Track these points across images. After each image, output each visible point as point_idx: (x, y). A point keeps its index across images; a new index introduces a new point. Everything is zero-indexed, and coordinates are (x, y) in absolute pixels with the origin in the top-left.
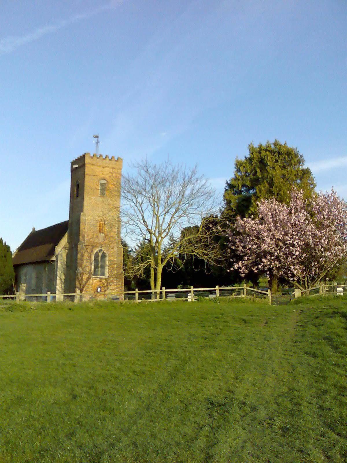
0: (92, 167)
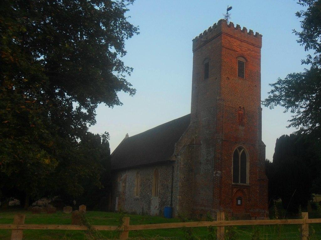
0: (229, 38)
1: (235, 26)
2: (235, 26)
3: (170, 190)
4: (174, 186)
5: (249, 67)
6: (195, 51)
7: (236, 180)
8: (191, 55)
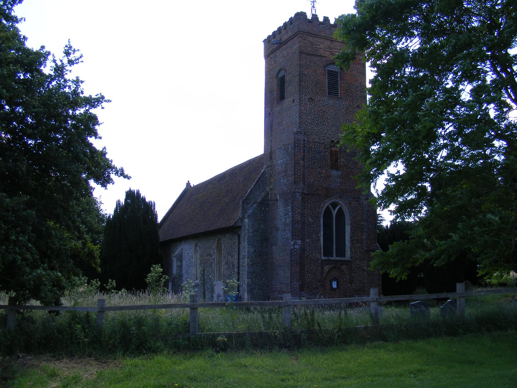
0: (310, 39)
1: (321, 19)
2: (321, 19)
3: (236, 270)
4: (240, 264)
5: (346, 79)
6: (265, 59)
7: (328, 252)
8: (264, 60)
